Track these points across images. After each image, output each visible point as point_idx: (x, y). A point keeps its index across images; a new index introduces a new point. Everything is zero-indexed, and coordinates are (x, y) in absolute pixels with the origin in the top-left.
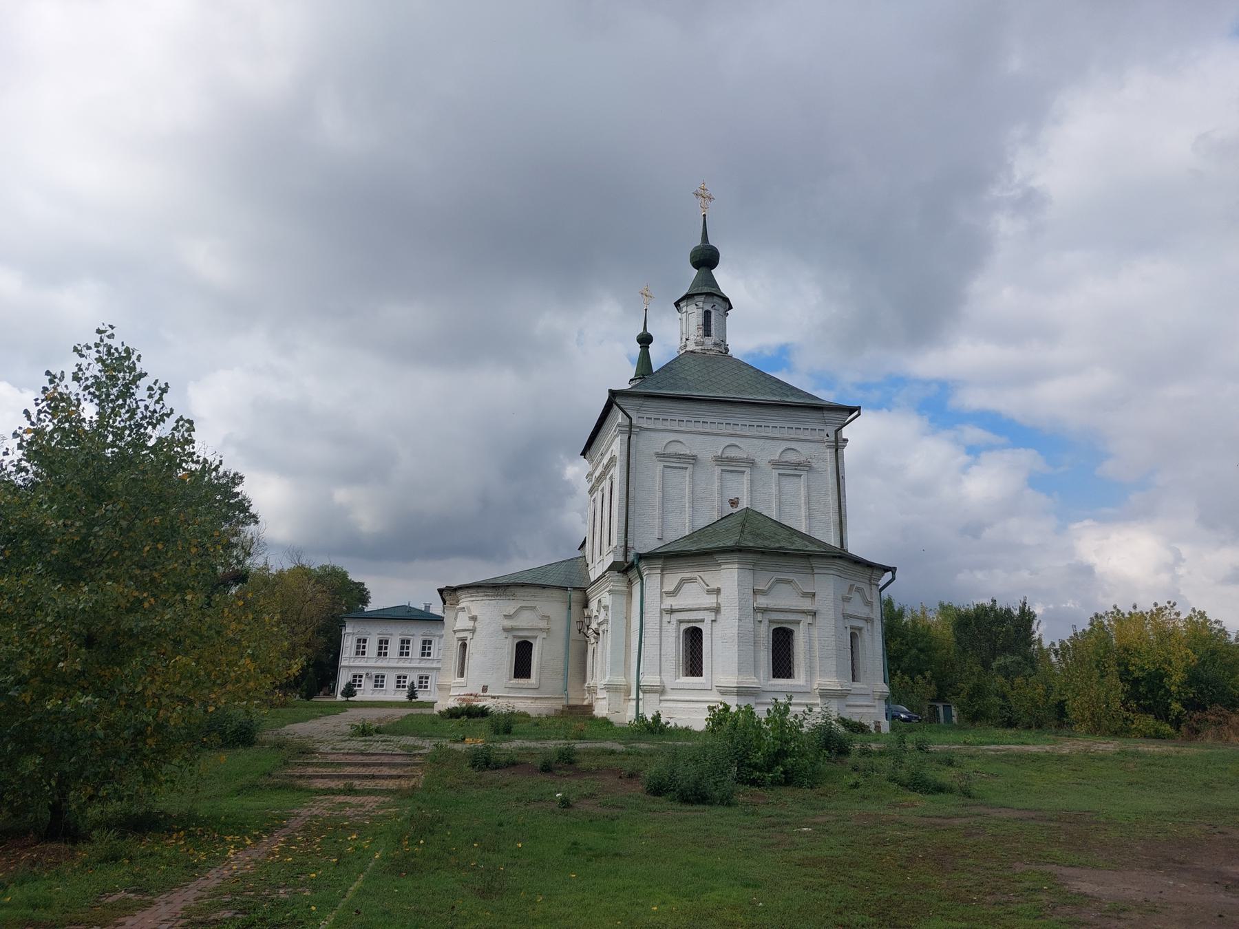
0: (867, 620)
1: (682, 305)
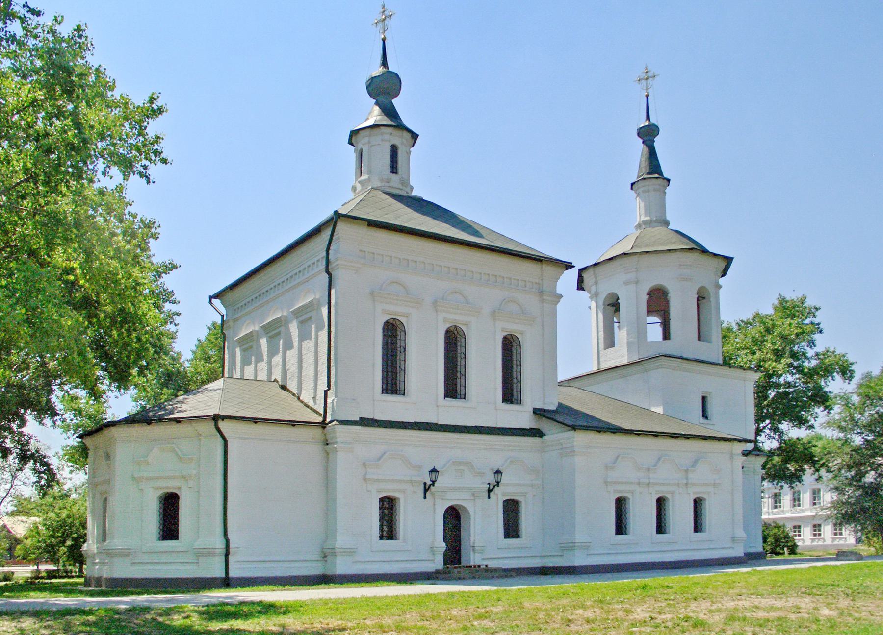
0: (715, 485)
1: (353, 141)
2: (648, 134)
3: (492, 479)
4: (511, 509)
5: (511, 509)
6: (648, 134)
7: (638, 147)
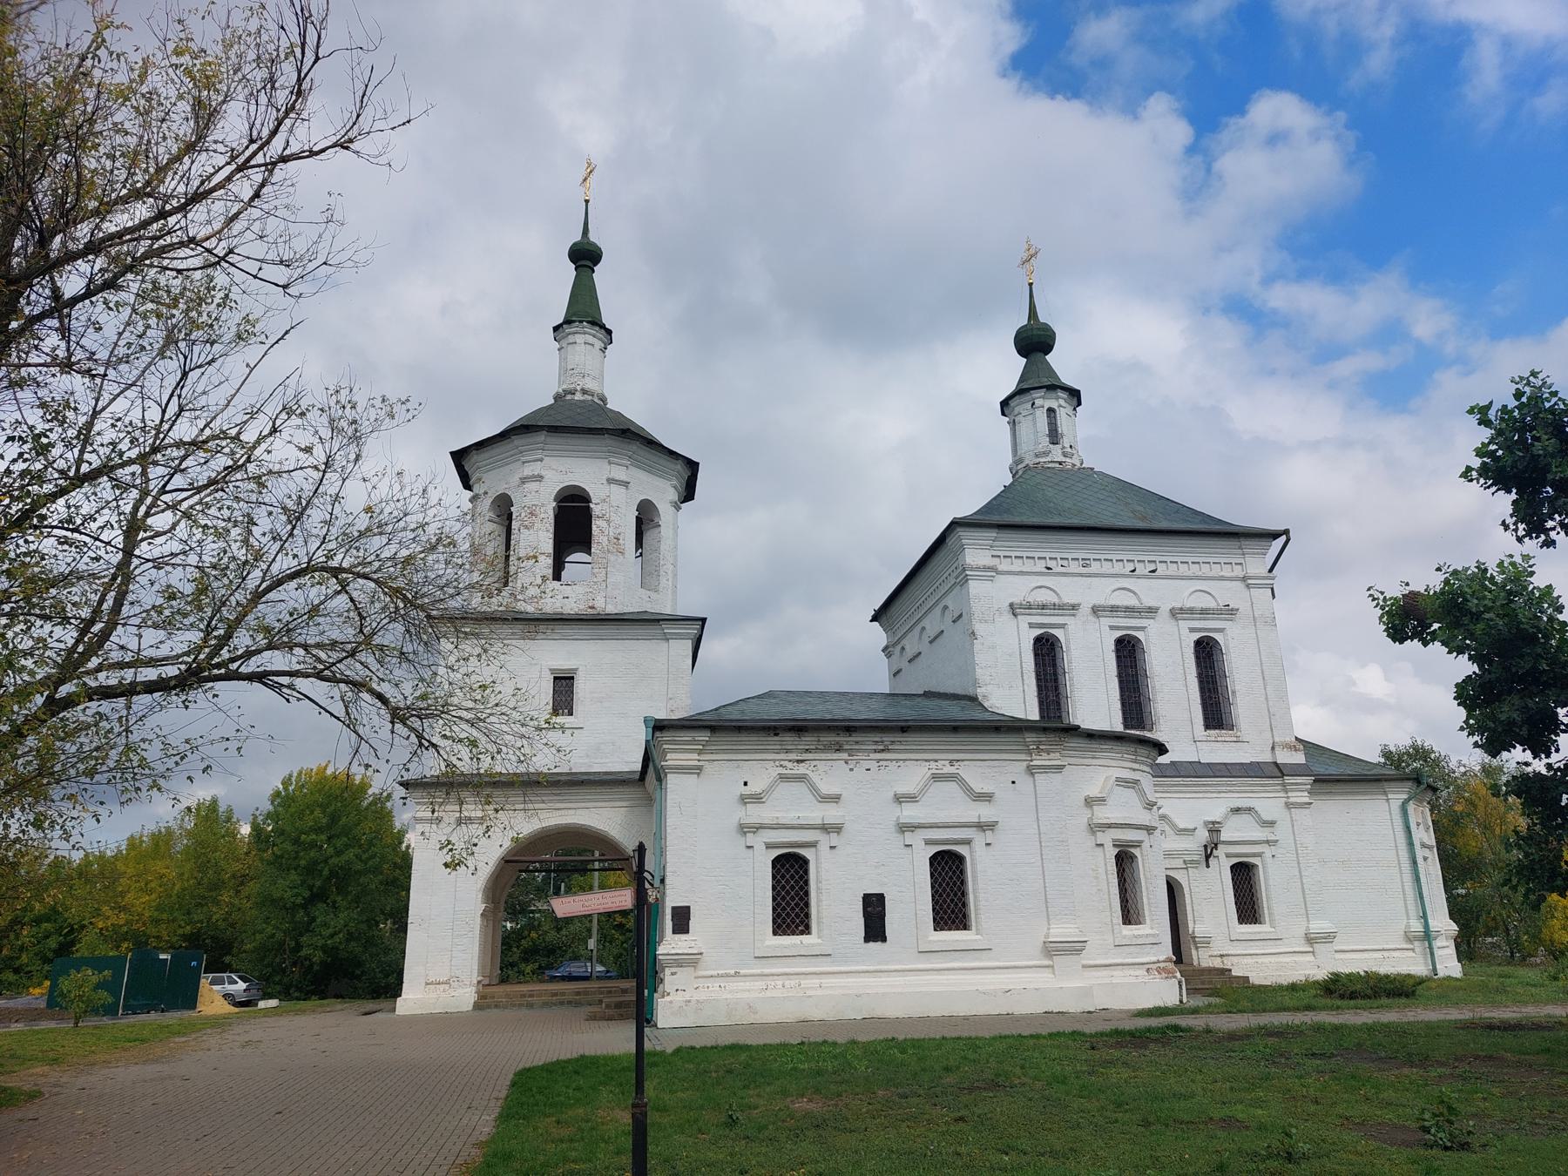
2: (585, 256)
3: (1203, 836)
4: (1243, 875)
5: (1243, 875)
6: (585, 256)
7: (570, 270)
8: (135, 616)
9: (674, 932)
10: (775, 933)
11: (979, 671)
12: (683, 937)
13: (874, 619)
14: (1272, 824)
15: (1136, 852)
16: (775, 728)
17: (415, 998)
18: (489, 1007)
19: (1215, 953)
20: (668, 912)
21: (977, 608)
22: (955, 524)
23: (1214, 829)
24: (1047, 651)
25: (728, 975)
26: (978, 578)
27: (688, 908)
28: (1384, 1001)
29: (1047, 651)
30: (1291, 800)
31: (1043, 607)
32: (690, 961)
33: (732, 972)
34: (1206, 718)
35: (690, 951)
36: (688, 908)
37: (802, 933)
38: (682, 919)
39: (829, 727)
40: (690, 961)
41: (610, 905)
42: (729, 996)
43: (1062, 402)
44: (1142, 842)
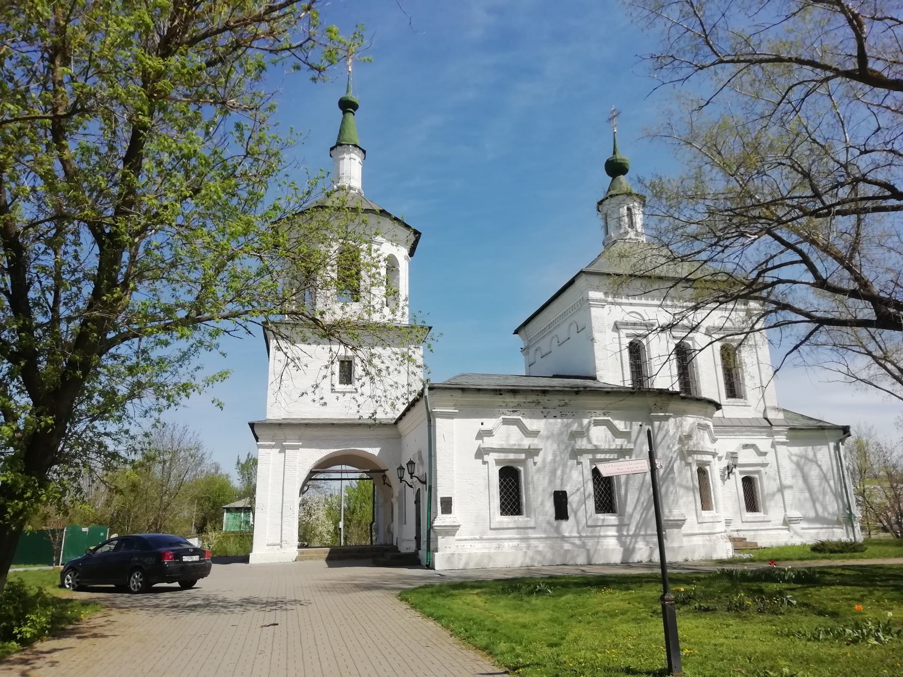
5: (749, 483)
8: (662, 265)
9: (443, 513)
10: (502, 514)
11: (597, 361)
12: (448, 516)
13: (516, 332)
14: (765, 454)
15: (708, 468)
16: (500, 390)
17: (259, 554)
18: (306, 559)
19: (734, 529)
20: (439, 500)
21: (595, 324)
22: (582, 272)
23: (733, 456)
24: (636, 351)
25: (475, 539)
26: (596, 306)
27: (451, 498)
28: (827, 555)
29: (636, 351)
30: (776, 440)
31: (635, 324)
32: (451, 531)
33: (478, 537)
34: (727, 393)
35: (454, 524)
36: (451, 498)
37: (517, 514)
38: (447, 506)
39: (532, 390)
40: (451, 531)
41: (635, 469)
42: (477, 551)
43: (636, 204)
44: (710, 462)
